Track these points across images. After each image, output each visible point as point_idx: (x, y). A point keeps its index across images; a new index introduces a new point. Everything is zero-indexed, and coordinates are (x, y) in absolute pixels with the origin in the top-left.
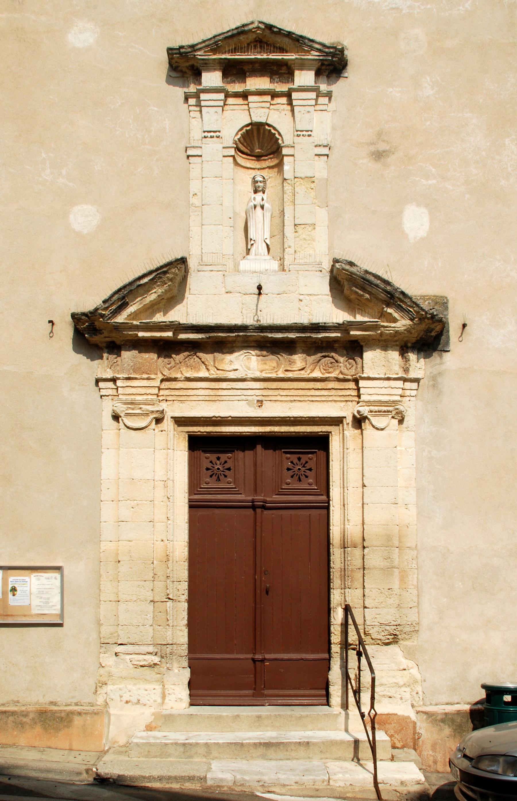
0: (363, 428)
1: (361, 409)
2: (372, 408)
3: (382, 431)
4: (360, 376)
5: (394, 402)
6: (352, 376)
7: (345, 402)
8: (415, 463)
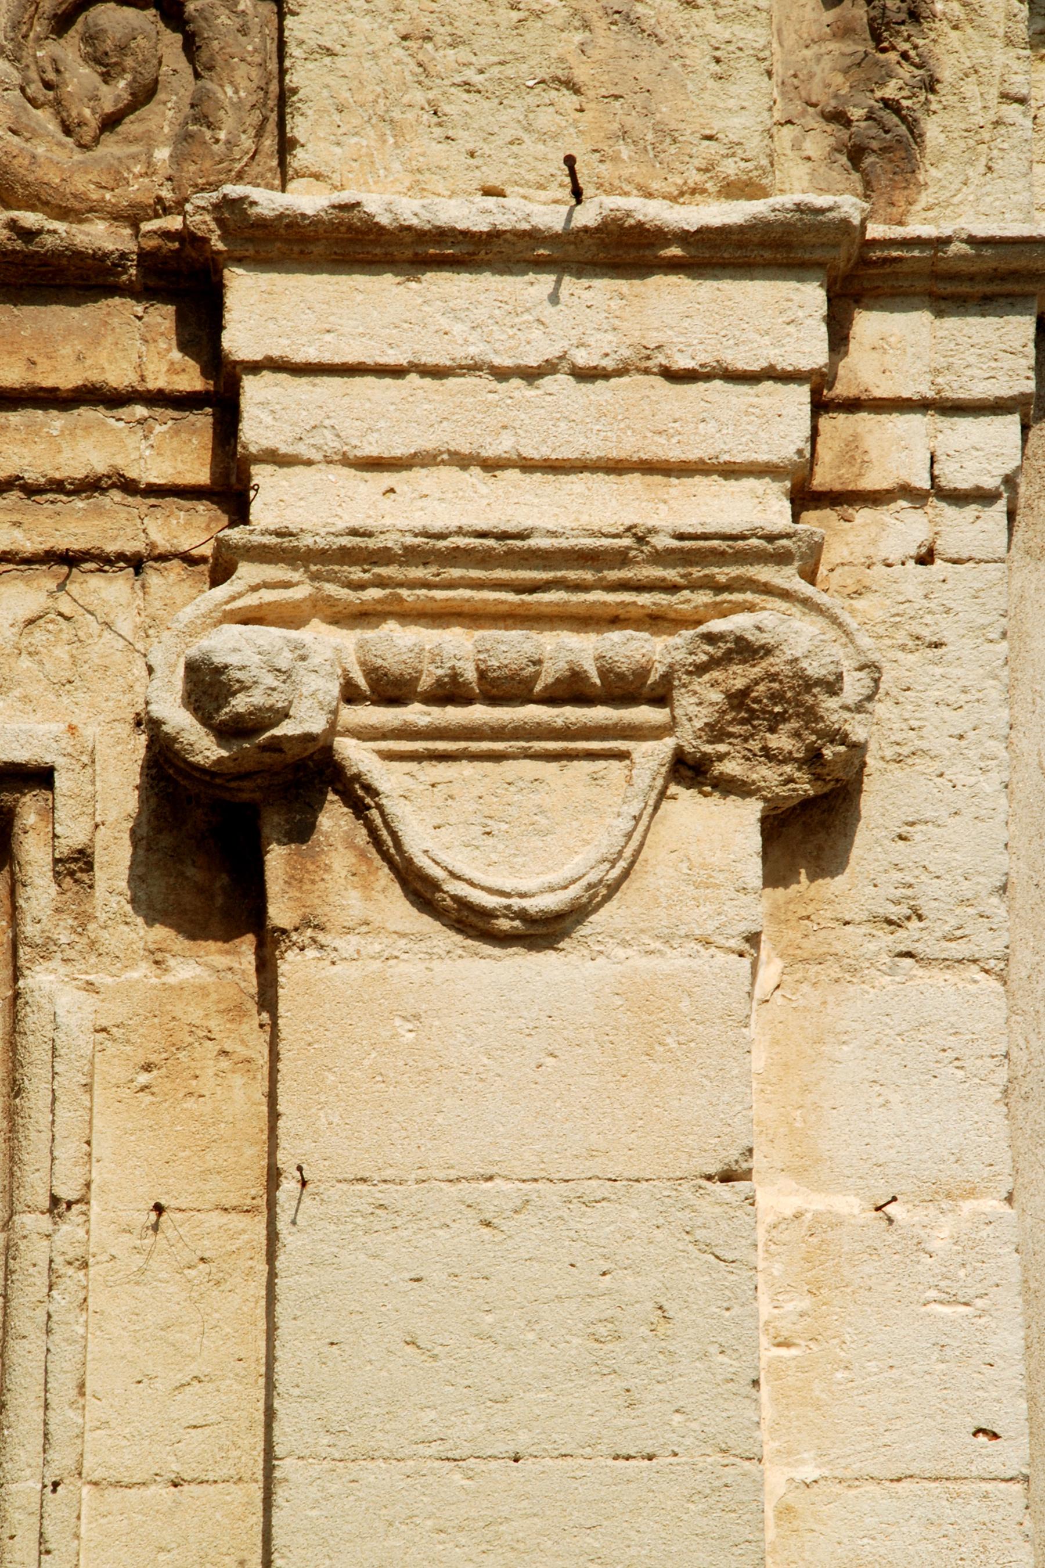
0: (280, 912)
1: (234, 646)
2: (400, 643)
3: (545, 960)
4: (231, 211)
5: (701, 555)
6: (131, 217)
7: (46, 579)
8: (1010, 1415)
